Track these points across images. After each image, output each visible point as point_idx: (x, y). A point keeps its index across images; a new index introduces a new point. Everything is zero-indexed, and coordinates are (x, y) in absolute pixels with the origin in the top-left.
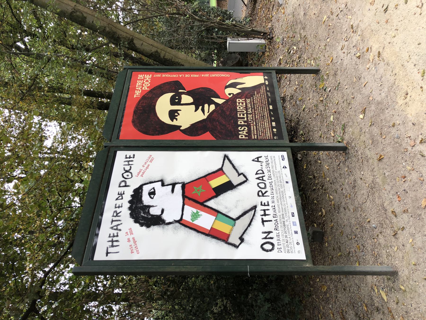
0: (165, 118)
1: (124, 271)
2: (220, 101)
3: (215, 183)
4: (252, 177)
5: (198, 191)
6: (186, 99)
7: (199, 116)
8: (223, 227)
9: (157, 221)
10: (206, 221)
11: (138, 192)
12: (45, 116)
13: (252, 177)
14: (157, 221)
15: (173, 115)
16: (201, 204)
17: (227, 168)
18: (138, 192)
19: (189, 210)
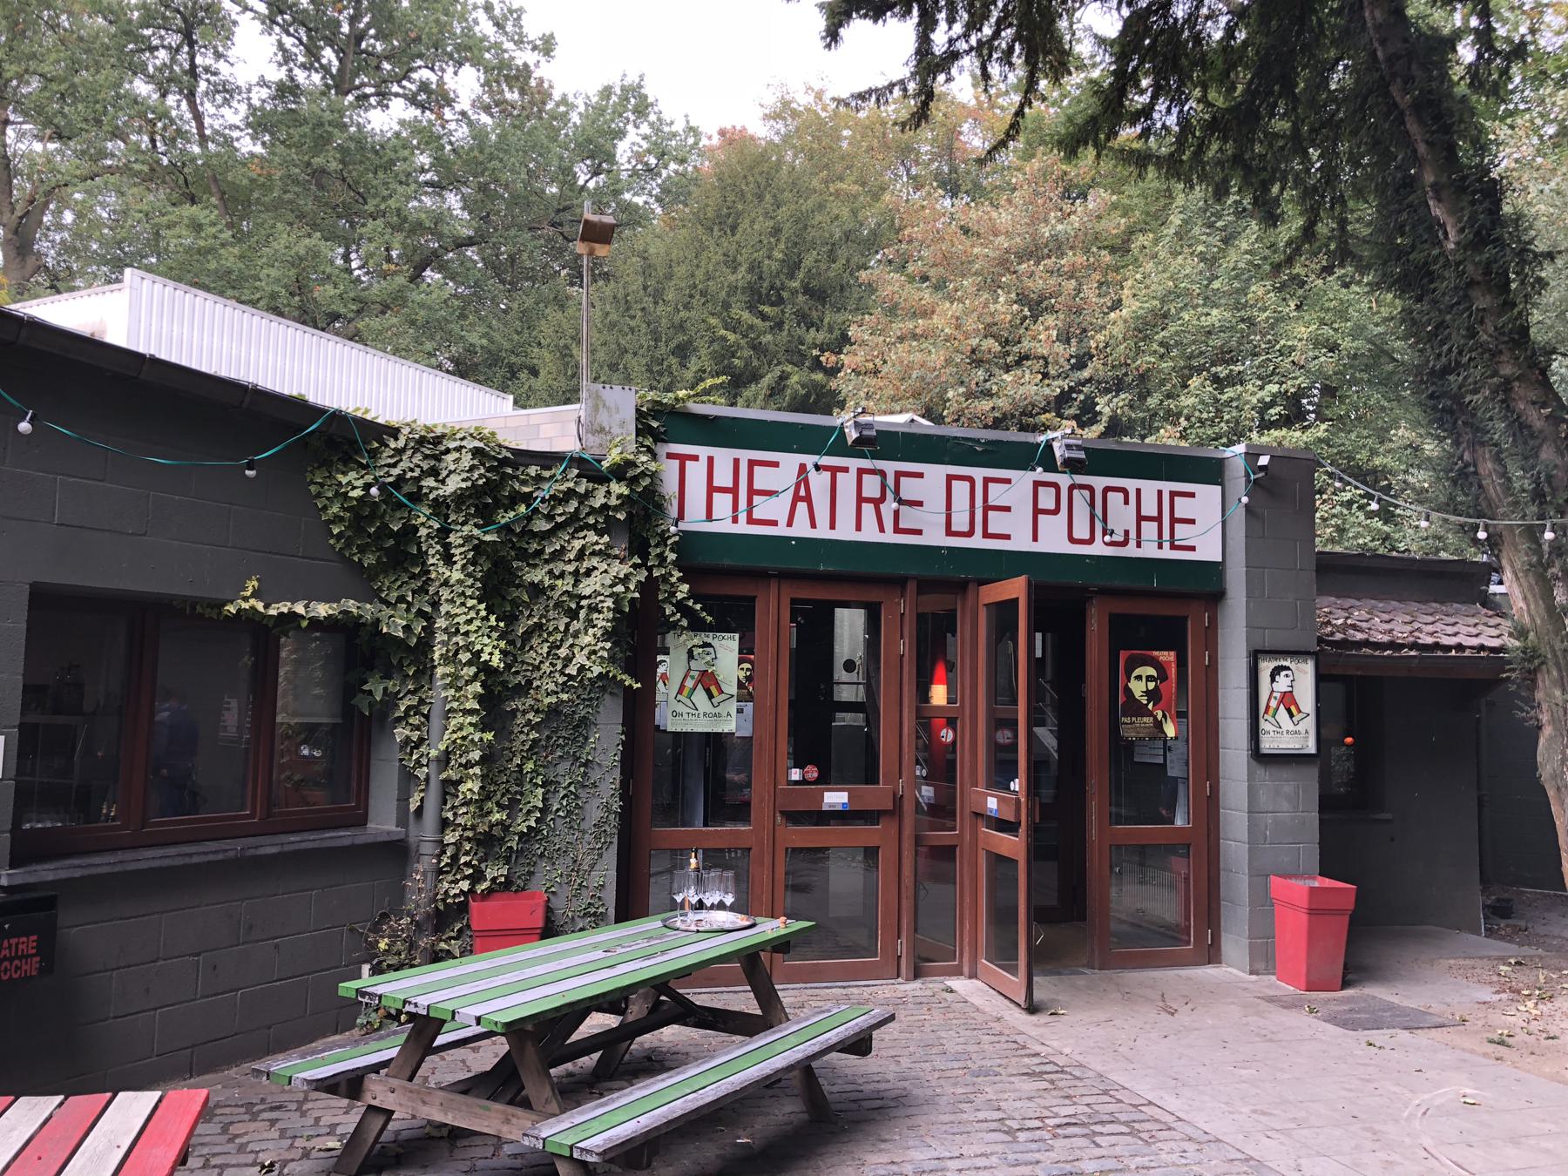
0: (1137, 672)
1: (1334, 672)
2: (1150, 706)
3: (1293, 709)
4: (717, 710)
5: (1287, 699)
6: (1151, 685)
7: (1138, 694)
8: (686, 692)
9: (1273, 680)
10: (690, 683)
11: (1288, 668)
12: (1453, 84)
13: (717, 710)
14: (1273, 680)
15: (1139, 678)
16: (1281, 701)
17: (723, 697)
18: (1288, 668)
19: (696, 674)
